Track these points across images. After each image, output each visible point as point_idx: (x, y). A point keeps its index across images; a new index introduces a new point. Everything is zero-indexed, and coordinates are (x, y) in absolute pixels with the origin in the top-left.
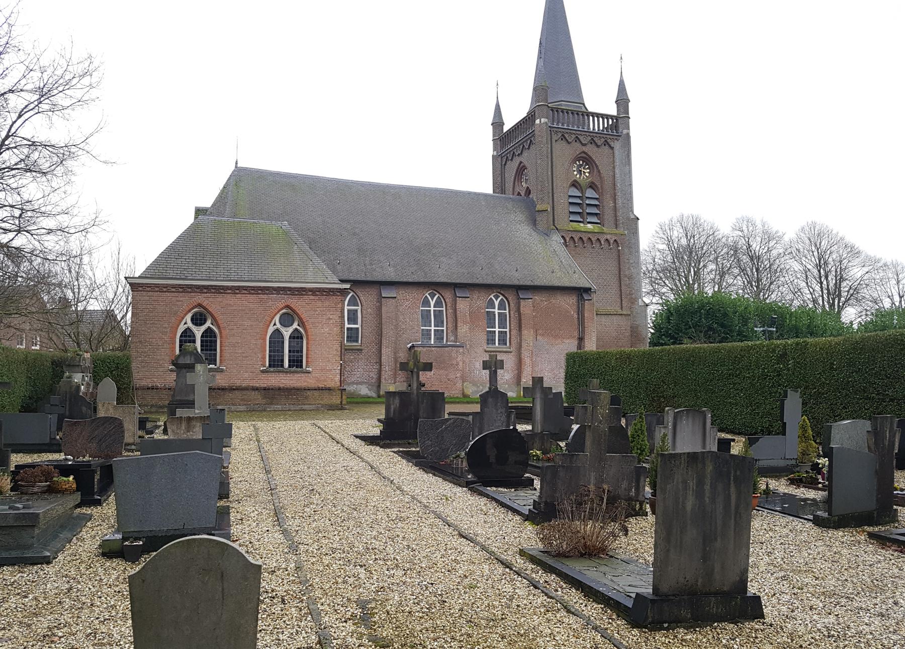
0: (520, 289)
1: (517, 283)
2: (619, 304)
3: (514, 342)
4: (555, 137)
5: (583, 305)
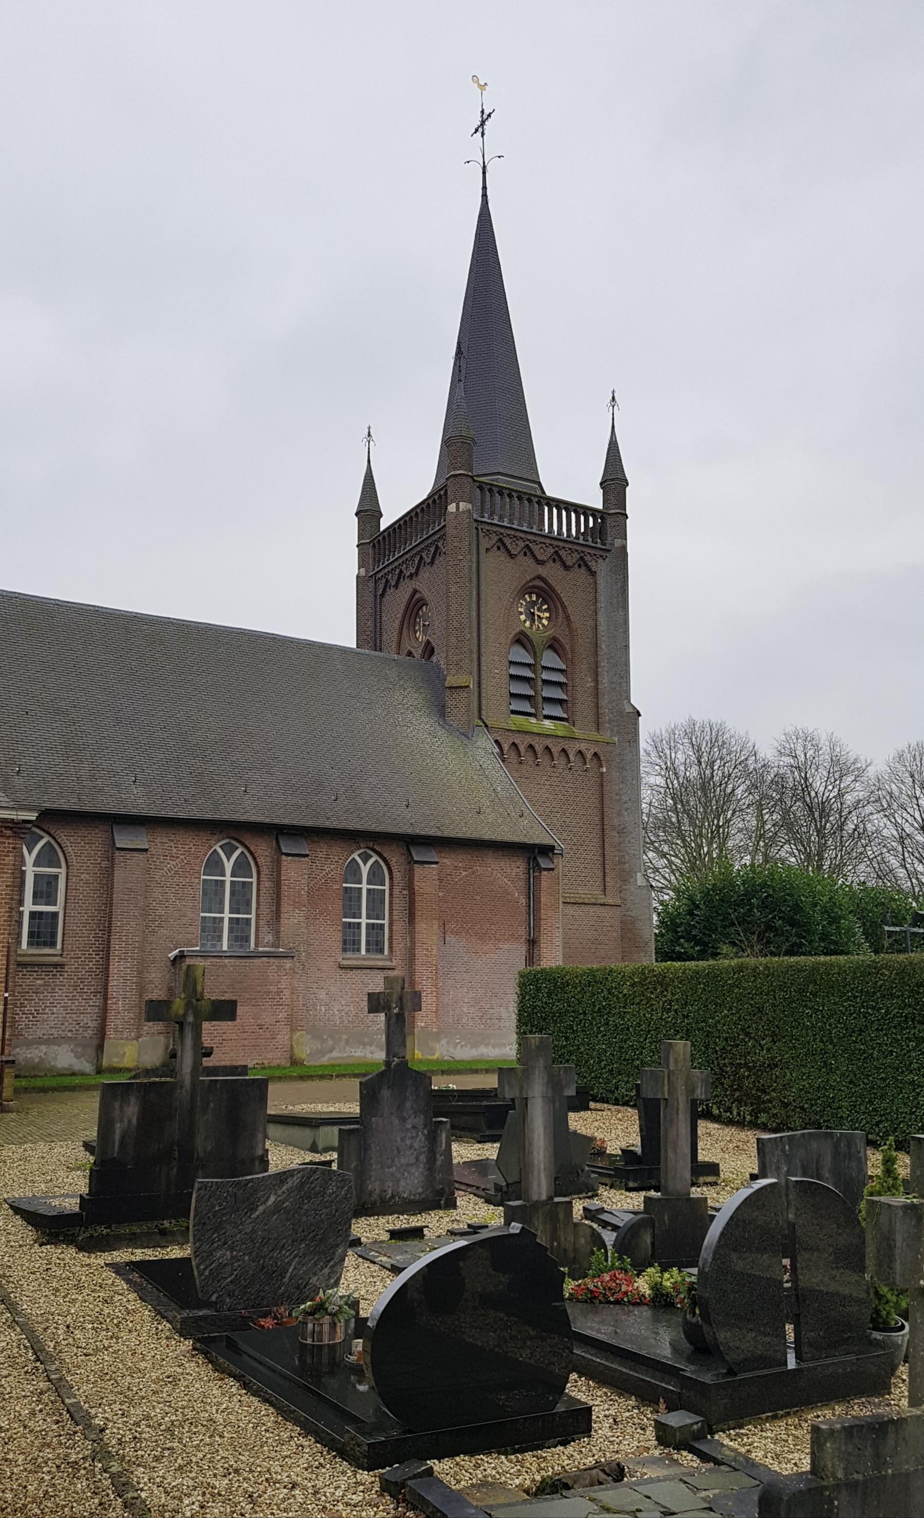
0: (411, 842)
1: (410, 831)
2: (599, 882)
3: (399, 947)
4: (485, 543)
5: (538, 880)
